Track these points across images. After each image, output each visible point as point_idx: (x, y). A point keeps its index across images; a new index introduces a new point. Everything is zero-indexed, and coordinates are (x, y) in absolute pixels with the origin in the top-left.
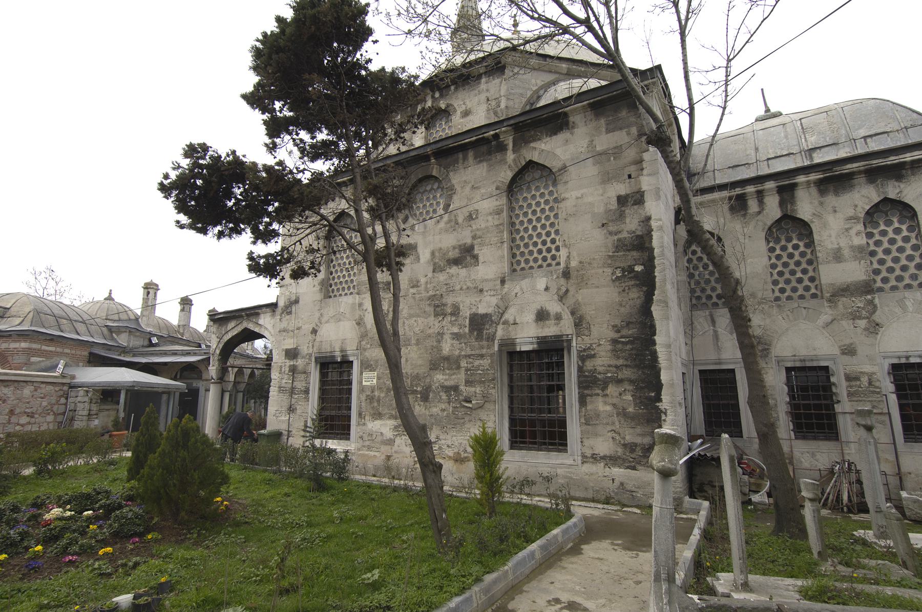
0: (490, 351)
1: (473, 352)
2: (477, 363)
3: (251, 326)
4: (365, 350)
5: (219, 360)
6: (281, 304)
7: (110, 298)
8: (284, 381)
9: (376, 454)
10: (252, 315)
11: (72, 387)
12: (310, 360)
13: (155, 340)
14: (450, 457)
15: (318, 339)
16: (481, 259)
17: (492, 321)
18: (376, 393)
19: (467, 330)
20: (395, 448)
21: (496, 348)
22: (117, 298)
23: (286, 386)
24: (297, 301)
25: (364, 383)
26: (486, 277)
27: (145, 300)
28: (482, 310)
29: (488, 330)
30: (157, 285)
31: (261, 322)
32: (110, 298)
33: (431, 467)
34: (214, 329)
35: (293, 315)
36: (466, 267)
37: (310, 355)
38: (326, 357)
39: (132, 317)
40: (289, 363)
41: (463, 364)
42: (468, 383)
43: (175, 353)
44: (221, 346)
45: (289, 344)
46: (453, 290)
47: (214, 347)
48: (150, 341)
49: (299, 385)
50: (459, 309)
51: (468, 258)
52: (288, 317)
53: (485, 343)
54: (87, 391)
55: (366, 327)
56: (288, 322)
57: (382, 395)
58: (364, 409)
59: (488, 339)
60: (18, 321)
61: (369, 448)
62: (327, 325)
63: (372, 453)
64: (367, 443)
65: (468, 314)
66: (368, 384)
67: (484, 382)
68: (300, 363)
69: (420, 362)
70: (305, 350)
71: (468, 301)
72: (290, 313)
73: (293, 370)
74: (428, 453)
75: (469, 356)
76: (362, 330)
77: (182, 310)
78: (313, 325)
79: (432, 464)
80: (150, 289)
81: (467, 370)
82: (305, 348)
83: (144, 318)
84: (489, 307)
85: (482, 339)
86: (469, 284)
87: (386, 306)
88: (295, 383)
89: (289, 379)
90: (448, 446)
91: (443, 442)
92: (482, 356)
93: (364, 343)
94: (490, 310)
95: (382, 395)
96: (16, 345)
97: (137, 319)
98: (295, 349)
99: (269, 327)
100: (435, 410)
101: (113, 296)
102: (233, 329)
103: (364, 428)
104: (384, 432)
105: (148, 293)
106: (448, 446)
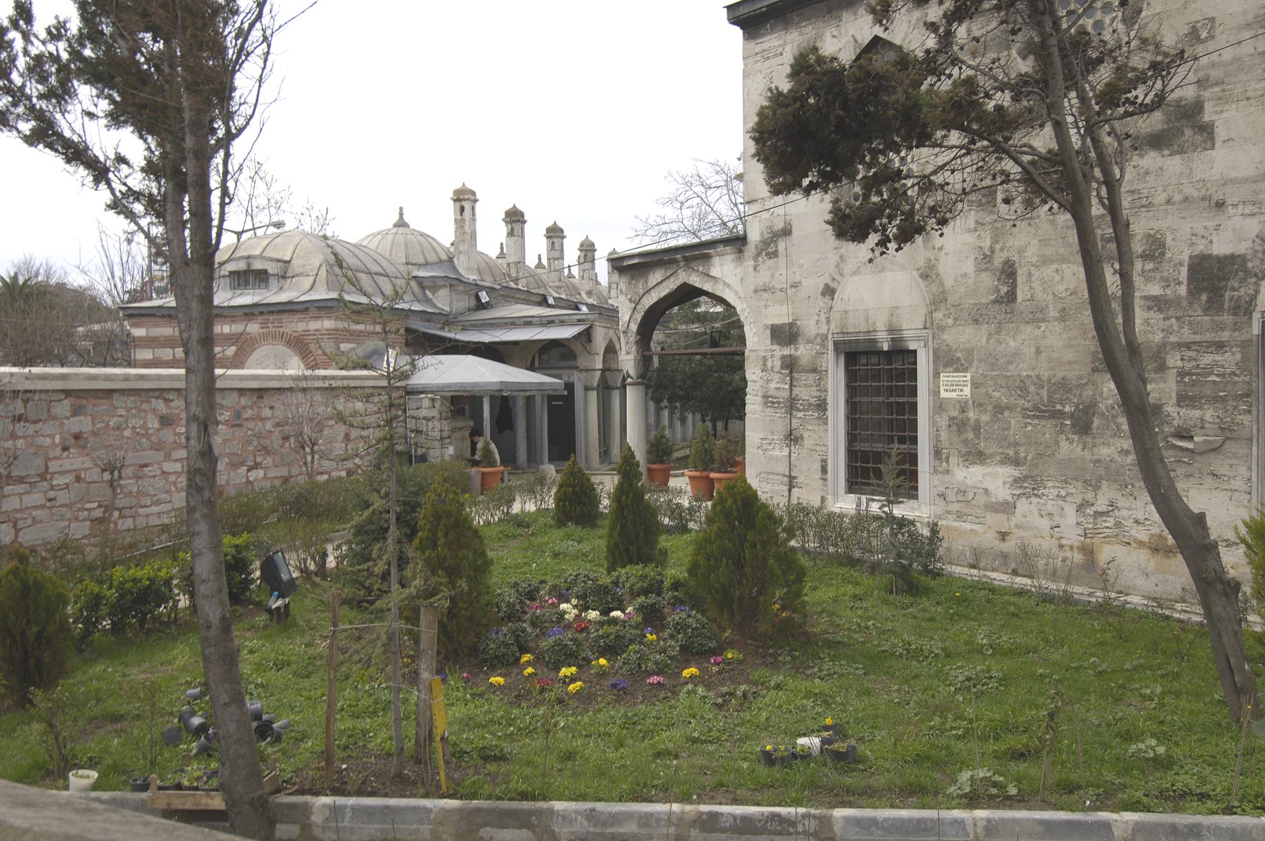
0: (1240, 336)
1: (1198, 338)
2: (1207, 359)
3: (696, 281)
4: (942, 329)
5: (637, 343)
6: (754, 236)
7: (401, 224)
8: (773, 385)
9: (976, 527)
10: (696, 258)
11: (411, 392)
12: (823, 345)
13: (484, 297)
14: (1141, 544)
15: (838, 305)
16: (1220, 132)
17: (1247, 272)
18: (972, 414)
19: (1183, 290)
20: (1017, 518)
21: (1256, 329)
22: (414, 222)
23: (779, 394)
24: (787, 232)
25: (943, 394)
26: (1233, 174)
27: (459, 223)
28: (1221, 247)
29: (1236, 290)
30: (473, 193)
31: (715, 271)
32: (401, 224)
33: (1220, 587)
34: (623, 283)
35: (782, 260)
36: (1181, 152)
37: (824, 338)
38: (857, 342)
39: (444, 257)
40: (780, 351)
41: (1174, 360)
42: (1184, 399)
43: (528, 322)
44: (639, 316)
45: (779, 315)
46: (1150, 205)
47: (626, 318)
48: (478, 298)
49: (805, 393)
50: (1162, 245)
51: (1188, 133)
52: (770, 262)
53: (1227, 318)
54: (433, 400)
55: (941, 284)
56: (775, 272)
57: (985, 418)
58: (945, 444)
59: (1235, 310)
60: (307, 283)
61: (960, 516)
62: (856, 278)
63: (968, 526)
64: (956, 507)
65: (1185, 257)
66: (953, 395)
67: (1223, 400)
68: (803, 351)
69: (1069, 355)
70: (810, 326)
71: (1185, 228)
72: (774, 254)
73: (790, 365)
74: (1212, 563)
75: (1188, 345)
76: (935, 288)
77: (511, 234)
78: (826, 279)
79: (1222, 582)
80: (464, 199)
81: (1182, 373)
82: (812, 323)
83: (462, 258)
84: (1240, 240)
85: (1220, 310)
86: (1189, 191)
87: (1112, 281)
88: (796, 391)
89: (783, 382)
90: (1137, 522)
91: (1125, 513)
92: (1220, 346)
93: (938, 315)
94: (1242, 248)
95: (985, 418)
96: (314, 325)
97: (451, 260)
98: (791, 325)
99: (734, 281)
100: (1105, 452)
101: (406, 218)
102: (660, 285)
103: (947, 478)
104: (991, 488)
105: (462, 209)
106: (1137, 522)
